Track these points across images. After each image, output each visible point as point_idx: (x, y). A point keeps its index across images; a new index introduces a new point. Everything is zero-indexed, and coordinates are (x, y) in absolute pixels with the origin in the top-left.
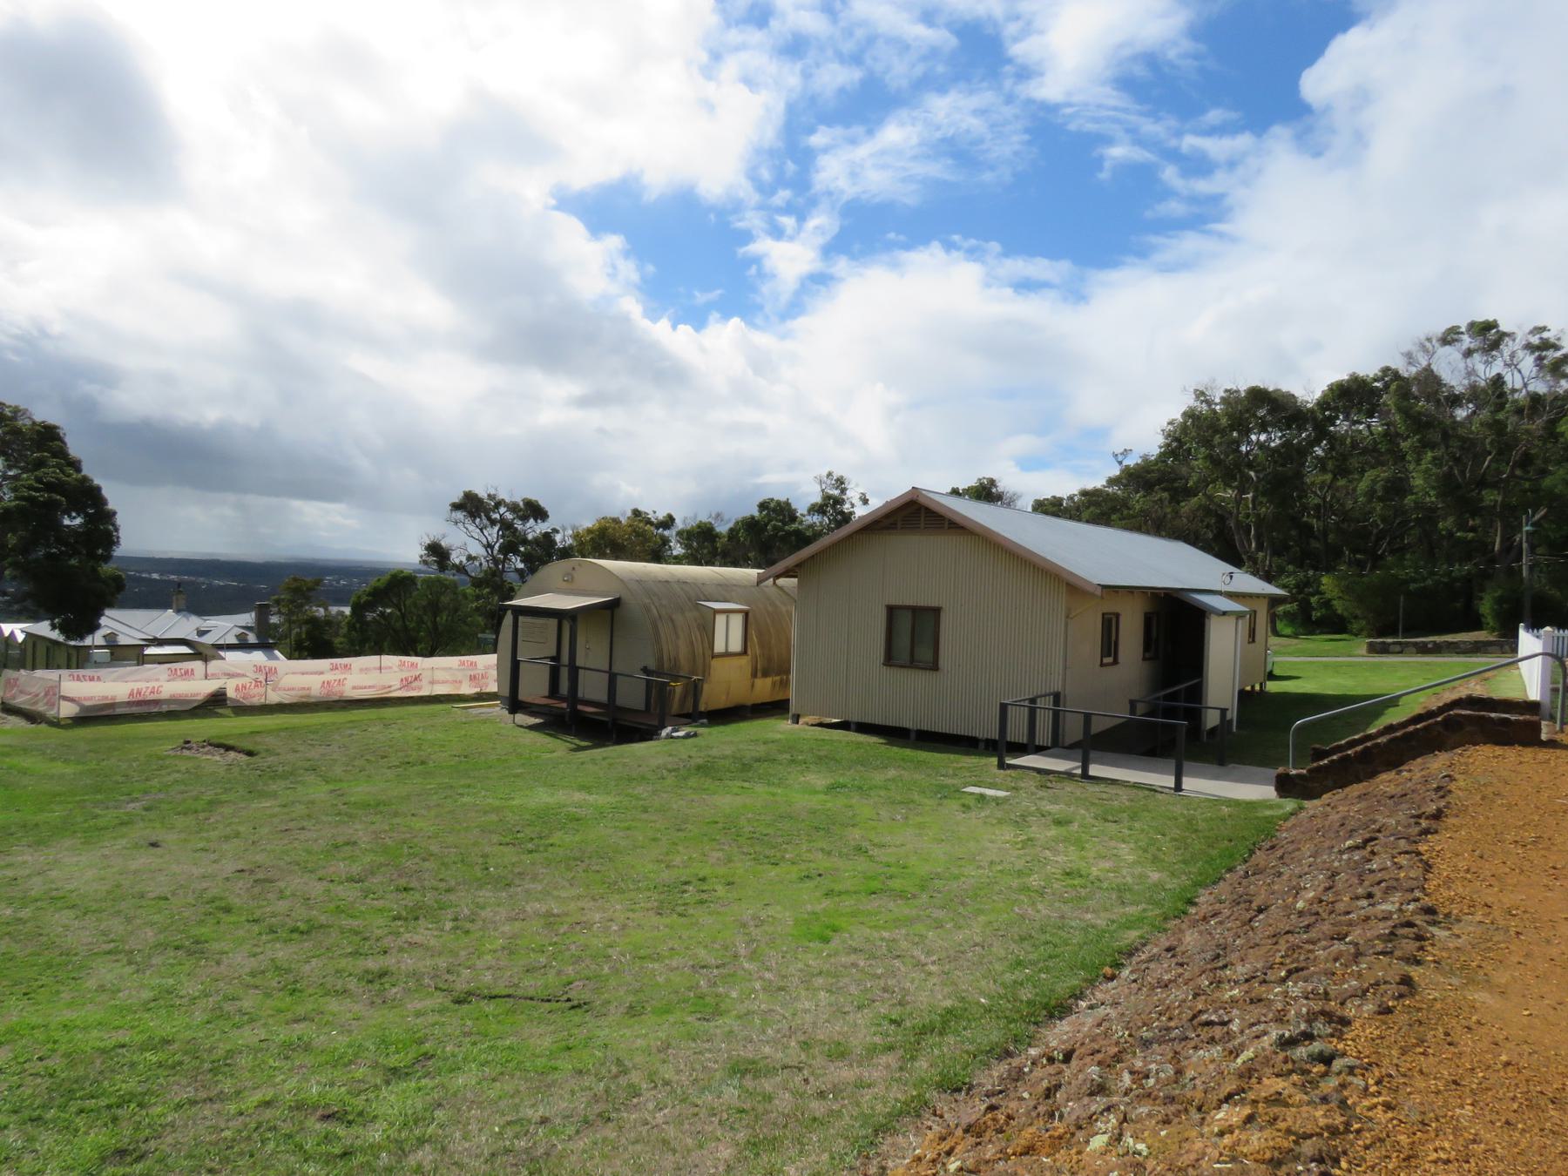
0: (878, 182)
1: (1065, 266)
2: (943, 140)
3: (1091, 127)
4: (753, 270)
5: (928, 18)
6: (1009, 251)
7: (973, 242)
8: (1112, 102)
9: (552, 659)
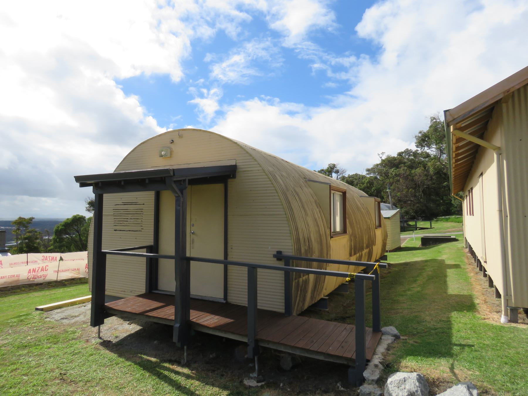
0: (232, 76)
1: (302, 105)
2: (253, 60)
3: (306, 57)
4: (196, 110)
5: (240, 8)
6: (283, 100)
7: (269, 97)
8: (313, 48)
9: (150, 249)
